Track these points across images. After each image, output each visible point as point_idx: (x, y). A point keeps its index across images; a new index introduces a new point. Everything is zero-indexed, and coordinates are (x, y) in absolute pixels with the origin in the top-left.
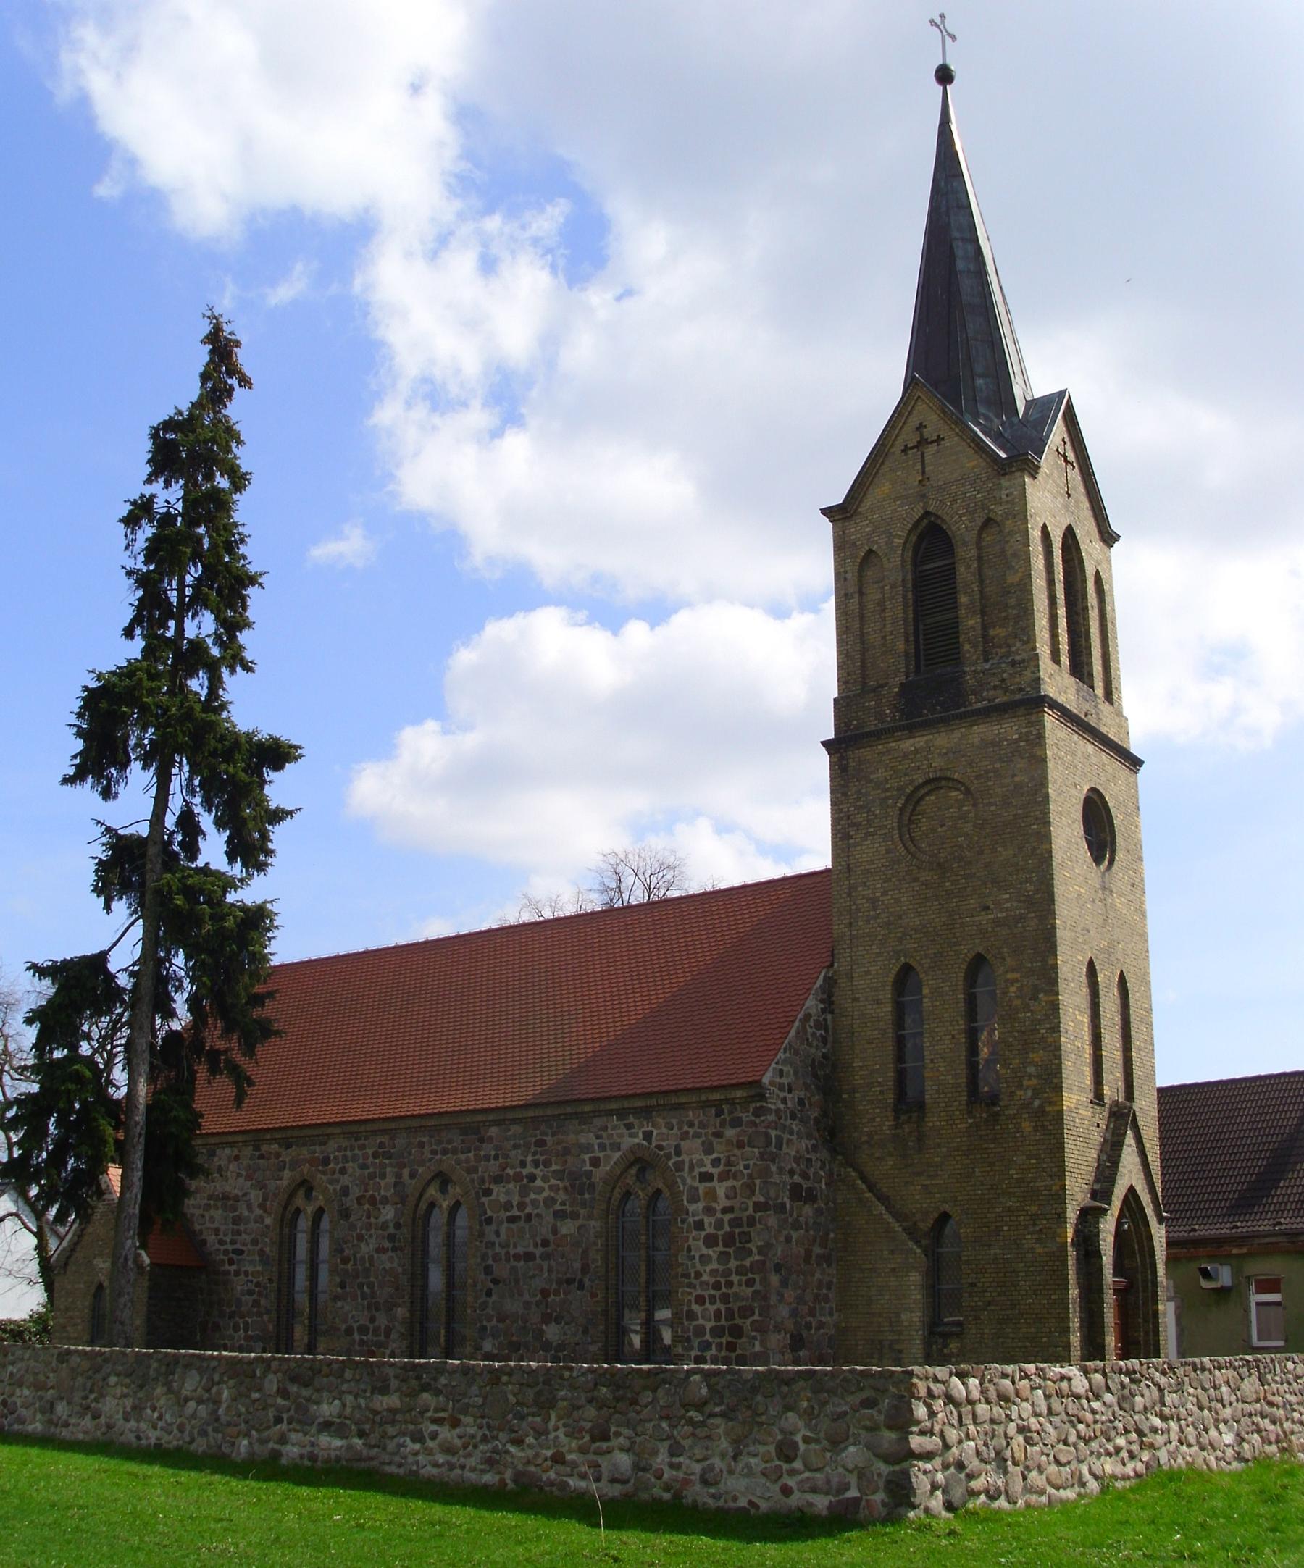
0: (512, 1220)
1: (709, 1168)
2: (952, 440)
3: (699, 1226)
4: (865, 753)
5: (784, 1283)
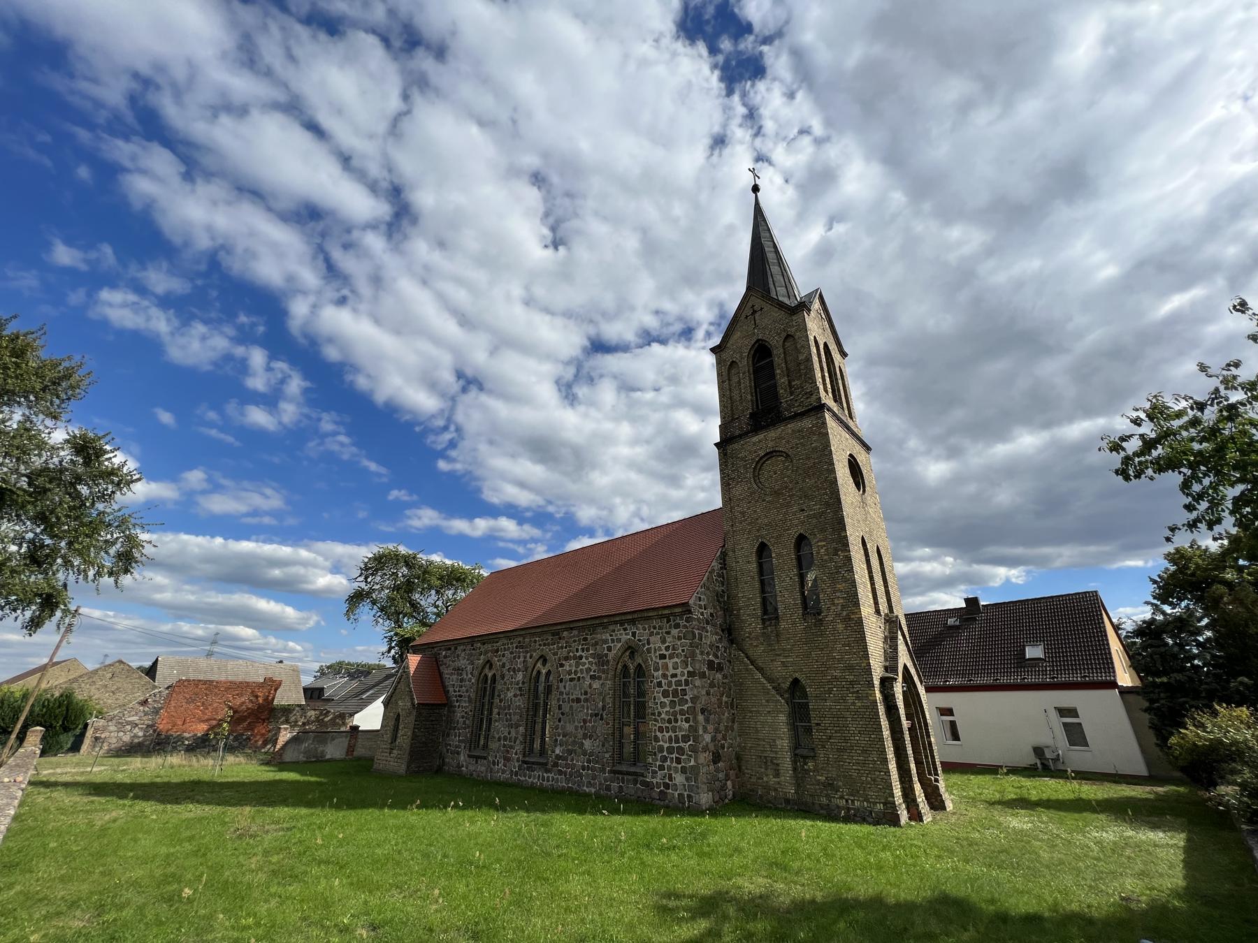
0: (571, 680)
1: (664, 652)
2: (767, 307)
3: (660, 685)
4: (736, 446)
5: (707, 720)
